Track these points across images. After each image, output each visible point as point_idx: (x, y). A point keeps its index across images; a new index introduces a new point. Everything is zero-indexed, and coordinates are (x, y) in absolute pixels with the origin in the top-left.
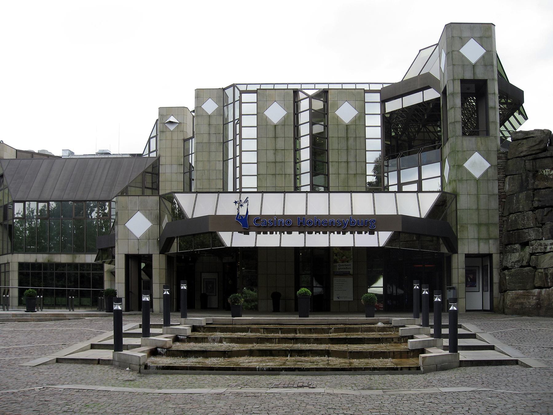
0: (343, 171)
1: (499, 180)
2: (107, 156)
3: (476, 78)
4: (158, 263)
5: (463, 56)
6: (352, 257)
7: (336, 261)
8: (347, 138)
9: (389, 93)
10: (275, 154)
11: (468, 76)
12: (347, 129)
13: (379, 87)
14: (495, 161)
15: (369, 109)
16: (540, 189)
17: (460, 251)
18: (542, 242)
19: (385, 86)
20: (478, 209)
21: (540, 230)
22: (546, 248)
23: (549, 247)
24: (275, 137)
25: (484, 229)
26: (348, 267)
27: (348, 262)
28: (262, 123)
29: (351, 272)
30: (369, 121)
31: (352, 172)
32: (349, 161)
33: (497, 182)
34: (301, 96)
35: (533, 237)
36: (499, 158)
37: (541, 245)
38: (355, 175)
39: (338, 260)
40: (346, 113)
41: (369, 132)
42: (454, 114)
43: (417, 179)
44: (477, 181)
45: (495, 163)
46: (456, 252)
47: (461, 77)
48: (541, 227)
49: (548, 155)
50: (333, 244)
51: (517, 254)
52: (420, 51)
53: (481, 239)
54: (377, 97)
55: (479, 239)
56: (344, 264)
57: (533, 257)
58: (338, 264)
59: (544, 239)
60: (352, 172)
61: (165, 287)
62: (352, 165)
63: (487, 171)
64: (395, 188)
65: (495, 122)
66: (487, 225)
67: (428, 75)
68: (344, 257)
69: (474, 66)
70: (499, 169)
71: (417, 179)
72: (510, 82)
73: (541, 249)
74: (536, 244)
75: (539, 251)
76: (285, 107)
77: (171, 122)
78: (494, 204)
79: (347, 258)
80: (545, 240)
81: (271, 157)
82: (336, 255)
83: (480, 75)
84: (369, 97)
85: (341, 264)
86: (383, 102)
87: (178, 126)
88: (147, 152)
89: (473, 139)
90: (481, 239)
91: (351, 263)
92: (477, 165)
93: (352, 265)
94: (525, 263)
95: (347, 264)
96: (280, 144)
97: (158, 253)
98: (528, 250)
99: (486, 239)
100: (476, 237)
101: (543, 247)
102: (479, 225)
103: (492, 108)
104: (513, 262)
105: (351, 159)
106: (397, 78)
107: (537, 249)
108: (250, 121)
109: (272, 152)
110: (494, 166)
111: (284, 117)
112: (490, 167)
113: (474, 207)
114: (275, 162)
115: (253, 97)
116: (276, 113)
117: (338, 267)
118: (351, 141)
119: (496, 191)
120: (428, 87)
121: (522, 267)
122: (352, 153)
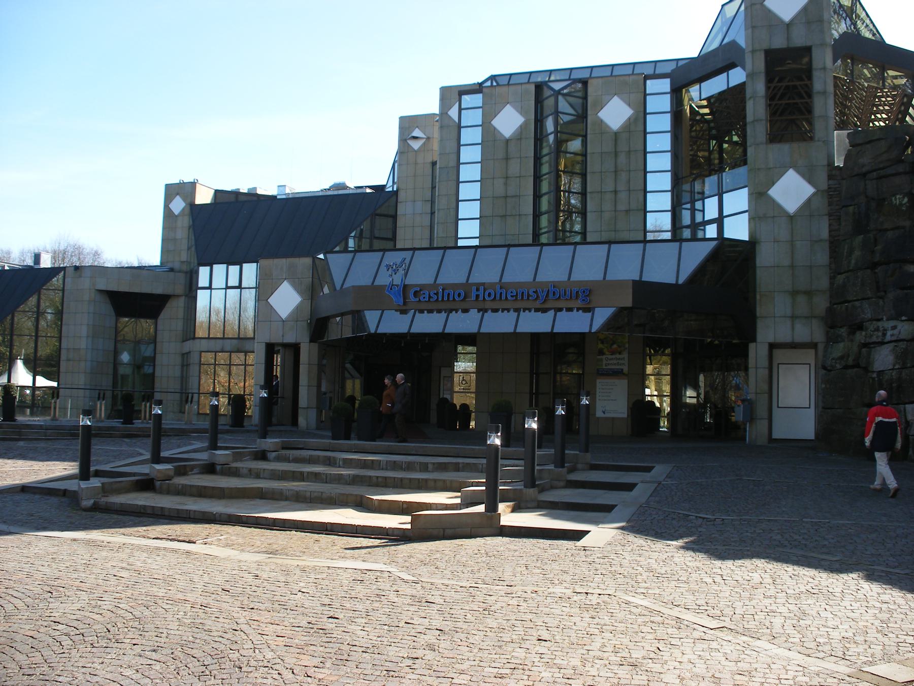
0: (608, 206)
1: (830, 215)
2: (341, 192)
3: (792, 45)
4: (308, 354)
5: (770, 11)
6: (627, 346)
7: (601, 353)
8: (616, 154)
9: (684, 75)
10: (506, 184)
11: (779, 42)
12: (616, 140)
13: (668, 69)
14: (824, 184)
15: (653, 104)
16: (887, 230)
17: (760, 336)
18: (880, 324)
19: (680, 63)
20: (792, 267)
21: (881, 302)
22: (884, 335)
23: (889, 333)
24: (507, 159)
25: (801, 299)
26: (620, 362)
27: (620, 353)
28: (490, 136)
29: (626, 370)
30: (653, 123)
31: (622, 207)
32: (618, 189)
33: (826, 218)
34: (547, 93)
35: (869, 316)
36: (830, 177)
37: (877, 330)
38: (627, 211)
39: (605, 350)
40: (614, 113)
41: (653, 143)
42: (756, 109)
43: (716, 216)
44: (791, 218)
45: (824, 186)
46: (754, 340)
47: (765, 46)
48: (881, 298)
49: (901, 170)
50: (559, 328)
51: (841, 345)
52: (723, 6)
53: (797, 317)
54: (665, 85)
55: (793, 317)
56: (613, 356)
57: (864, 350)
58: (604, 357)
59: (885, 319)
60: (622, 207)
61: (262, 388)
62: (623, 196)
63: (809, 201)
64: (578, 239)
65: (825, 117)
66: (809, 293)
67: (733, 43)
68: (615, 346)
69: (789, 25)
70: (830, 197)
71: (716, 216)
72: (889, 40)
73: (877, 337)
74: (872, 326)
75: (874, 339)
76: (522, 112)
77: (415, 138)
78: (822, 257)
79: (619, 346)
80: (888, 320)
81: (500, 190)
82: (602, 343)
83: (799, 39)
84: (652, 86)
85: (610, 357)
86: (677, 92)
87: (424, 143)
88: (390, 183)
89: (785, 147)
90: (797, 317)
91: (625, 355)
92: (792, 191)
93: (626, 359)
94: (850, 361)
95: (618, 356)
96: (514, 168)
97: (308, 340)
98: (860, 337)
99: (806, 317)
100: (789, 313)
101: (880, 334)
102: (794, 293)
103: (819, 93)
104: (833, 359)
105: (621, 187)
106: (692, 51)
107: (871, 336)
108: (471, 135)
109: (502, 181)
110: (823, 191)
111: (521, 126)
112: (814, 195)
113: (787, 262)
114: (506, 197)
115: (475, 100)
116: (510, 121)
117: (604, 362)
118: (622, 159)
119: (825, 234)
120: (732, 66)
121: (846, 367)
122: (623, 176)
